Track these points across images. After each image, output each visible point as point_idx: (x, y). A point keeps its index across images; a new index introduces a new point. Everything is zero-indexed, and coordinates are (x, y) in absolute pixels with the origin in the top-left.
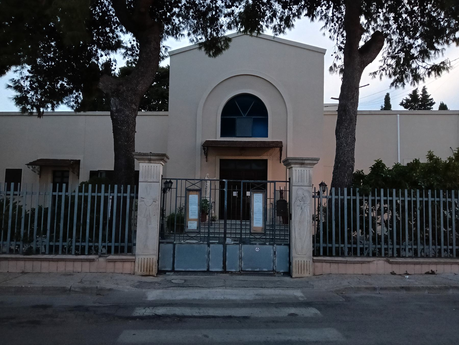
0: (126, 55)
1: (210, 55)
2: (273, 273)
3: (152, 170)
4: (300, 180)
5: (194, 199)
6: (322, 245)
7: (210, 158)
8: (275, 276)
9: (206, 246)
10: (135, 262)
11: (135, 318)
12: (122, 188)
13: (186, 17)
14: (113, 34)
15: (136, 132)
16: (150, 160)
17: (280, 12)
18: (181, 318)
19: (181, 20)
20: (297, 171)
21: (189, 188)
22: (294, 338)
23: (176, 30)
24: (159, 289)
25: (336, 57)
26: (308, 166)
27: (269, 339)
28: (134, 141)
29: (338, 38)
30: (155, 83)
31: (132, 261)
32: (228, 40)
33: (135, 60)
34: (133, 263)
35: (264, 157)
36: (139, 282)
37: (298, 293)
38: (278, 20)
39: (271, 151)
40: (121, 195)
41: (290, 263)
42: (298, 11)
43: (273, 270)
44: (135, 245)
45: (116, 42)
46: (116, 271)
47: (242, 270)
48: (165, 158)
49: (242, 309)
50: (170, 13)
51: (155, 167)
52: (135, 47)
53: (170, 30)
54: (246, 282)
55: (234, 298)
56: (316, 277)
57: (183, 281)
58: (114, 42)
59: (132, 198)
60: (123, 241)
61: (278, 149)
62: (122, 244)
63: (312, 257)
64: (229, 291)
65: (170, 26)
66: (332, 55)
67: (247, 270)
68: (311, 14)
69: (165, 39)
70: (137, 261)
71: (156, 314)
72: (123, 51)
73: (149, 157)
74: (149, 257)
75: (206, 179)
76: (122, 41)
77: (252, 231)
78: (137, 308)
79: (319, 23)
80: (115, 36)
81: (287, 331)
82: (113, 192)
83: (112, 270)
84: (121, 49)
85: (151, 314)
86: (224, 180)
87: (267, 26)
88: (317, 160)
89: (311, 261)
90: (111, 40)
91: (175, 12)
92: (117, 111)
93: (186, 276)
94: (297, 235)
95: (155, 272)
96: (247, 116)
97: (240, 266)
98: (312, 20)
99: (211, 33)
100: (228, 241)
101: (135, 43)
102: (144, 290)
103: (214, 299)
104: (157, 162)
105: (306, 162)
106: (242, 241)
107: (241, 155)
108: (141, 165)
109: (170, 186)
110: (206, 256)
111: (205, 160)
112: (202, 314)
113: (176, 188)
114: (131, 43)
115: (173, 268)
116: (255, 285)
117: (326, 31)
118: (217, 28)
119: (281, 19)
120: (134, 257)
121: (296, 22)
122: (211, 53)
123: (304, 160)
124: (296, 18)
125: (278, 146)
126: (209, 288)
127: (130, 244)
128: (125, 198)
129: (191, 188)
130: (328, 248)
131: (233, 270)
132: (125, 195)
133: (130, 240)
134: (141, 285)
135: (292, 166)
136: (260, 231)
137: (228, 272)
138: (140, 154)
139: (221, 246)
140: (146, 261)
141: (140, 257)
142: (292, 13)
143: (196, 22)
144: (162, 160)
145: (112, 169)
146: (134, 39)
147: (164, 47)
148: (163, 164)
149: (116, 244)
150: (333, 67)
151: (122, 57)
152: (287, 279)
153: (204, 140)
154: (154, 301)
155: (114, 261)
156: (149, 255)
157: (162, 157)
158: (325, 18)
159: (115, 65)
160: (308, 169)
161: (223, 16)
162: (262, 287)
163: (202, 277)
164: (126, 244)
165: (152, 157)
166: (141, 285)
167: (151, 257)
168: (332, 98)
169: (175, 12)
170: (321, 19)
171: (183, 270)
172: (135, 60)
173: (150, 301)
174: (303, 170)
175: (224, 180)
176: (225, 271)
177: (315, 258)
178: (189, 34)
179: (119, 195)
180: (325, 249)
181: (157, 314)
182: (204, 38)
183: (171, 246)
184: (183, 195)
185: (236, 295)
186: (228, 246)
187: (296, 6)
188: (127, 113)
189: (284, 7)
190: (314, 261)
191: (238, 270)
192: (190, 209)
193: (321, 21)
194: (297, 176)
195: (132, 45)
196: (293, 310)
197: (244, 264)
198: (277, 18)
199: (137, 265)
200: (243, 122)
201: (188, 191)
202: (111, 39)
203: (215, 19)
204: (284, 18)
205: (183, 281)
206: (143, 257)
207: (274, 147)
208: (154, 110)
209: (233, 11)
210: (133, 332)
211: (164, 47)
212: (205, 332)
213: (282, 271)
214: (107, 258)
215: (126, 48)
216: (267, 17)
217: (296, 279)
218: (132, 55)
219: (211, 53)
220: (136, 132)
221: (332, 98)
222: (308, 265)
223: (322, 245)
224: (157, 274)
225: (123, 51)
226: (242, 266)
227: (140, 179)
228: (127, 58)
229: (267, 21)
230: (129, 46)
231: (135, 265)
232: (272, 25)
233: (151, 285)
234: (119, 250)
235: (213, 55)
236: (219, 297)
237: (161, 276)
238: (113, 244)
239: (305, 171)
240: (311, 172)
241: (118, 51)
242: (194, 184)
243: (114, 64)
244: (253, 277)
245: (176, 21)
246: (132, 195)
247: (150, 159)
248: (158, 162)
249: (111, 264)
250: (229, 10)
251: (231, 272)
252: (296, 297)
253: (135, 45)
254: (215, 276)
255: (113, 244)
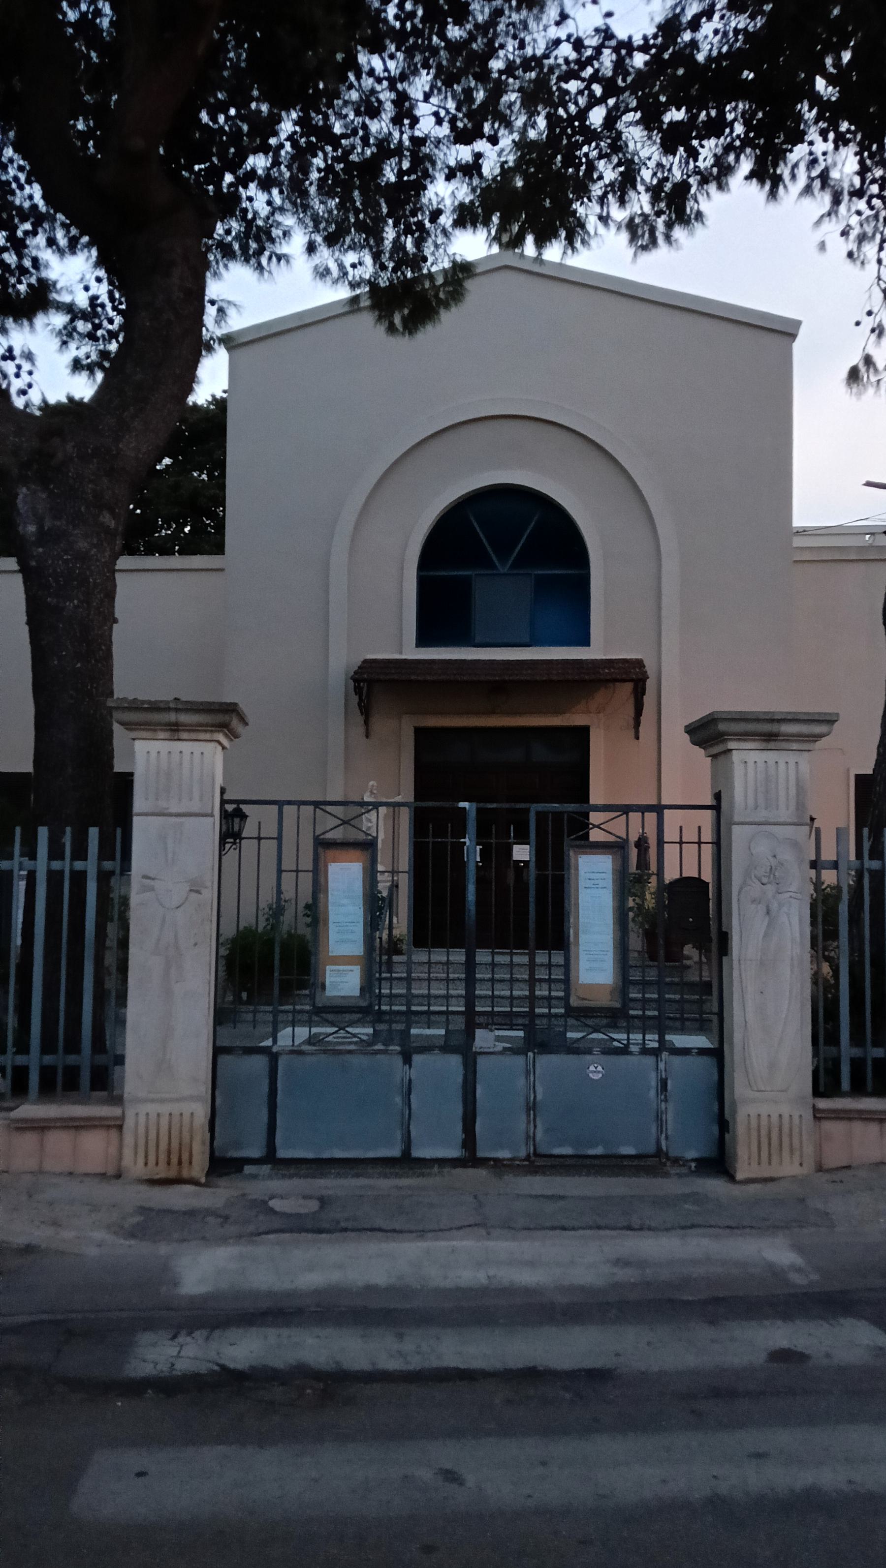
0: (70, 335)
1: (391, 329)
2: (653, 1162)
3: (186, 765)
4: (761, 801)
5: (345, 878)
6: (847, 1050)
7: (379, 724)
8: (666, 1175)
9: (398, 1061)
10: (120, 1128)
11: (136, 1388)
12: (67, 840)
13: (296, 191)
14: (20, 256)
15: (115, 621)
16: (175, 730)
17: (652, 164)
18: (332, 1386)
19: (278, 200)
20: (751, 764)
21: (329, 836)
22: (830, 1478)
23: (258, 240)
24: (224, 1240)
25: (873, 331)
26: (795, 746)
27: (723, 1489)
28: (109, 655)
29: (882, 254)
30: (167, 461)
31: (109, 1127)
32: (462, 271)
33: (104, 354)
34: (114, 1133)
35: (578, 720)
36: (143, 1210)
37: (777, 1253)
38: (645, 198)
39: (600, 697)
40: (65, 865)
41: (724, 1125)
42: (719, 161)
43: (659, 1152)
44: (120, 1060)
45: (30, 286)
46: (48, 1165)
47: (536, 1154)
48: (235, 722)
49: (253, 1056)
50: (233, 172)
51: (197, 755)
52: (103, 306)
53: (236, 238)
54: (561, 1203)
55: (526, 1278)
56: (827, 1177)
57: (314, 1205)
58: (22, 288)
59: (104, 878)
60: (73, 1046)
61: (629, 686)
62: (72, 1059)
63: (810, 1099)
64: (502, 1246)
65: (235, 225)
66: (858, 324)
67: (557, 1151)
68: (766, 174)
69: (215, 274)
70: (129, 1123)
71: (223, 1367)
72: (59, 320)
73: (172, 717)
74: (175, 1108)
75: (366, 799)
76: (55, 283)
77: (574, 1002)
78: (145, 1338)
79: (799, 208)
80: (27, 263)
81: (783, 1438)
82: (33, 856)
83: (32, 1164)
84: (52, 311)
85: (203, 1368)
86: (462, 804)
87: (604, 219)
88: (830, 720)
89: (808, 1115)
90: (13, 280)
91: (253, 170)
92: (44, 537)
93: (322, 1182)
94: (750, 1016)
95: (199, 1167)
96: (513, 567)
97: (530, 1138)
98: (773, 194)
99: (396, 241)
100: (483, 1039)
101: (102, 290)
102: (164, 1249)
103: (448, 1284)
104: (202, 736)
105: (786, 728)
106: (539, 1041)
107: (492, 712)
108: (141, 747)
109: (236, 828)
110: (398, 1100)
111: (361, 730)
112: (415, 1363)
113: (279, 839)
114: (87, 289)
115: (271, 1146)
116: (600, 1220)
117: (833, 228)
118: (420, 224)
119: (655, 192)
120: (116, 1111)
121: (710, 202)
122: (397, 320)
123: (779, 721)
124: (712, 188)
125: (632, 677)
126: (422, 1234)
127: (101, 1059)
128: (79, 878)
129: (336, 835)
130: (869, 1063)
131: (504, 1154)
132: (79, 865)
133: (99, 1043)
134: (149, 1224)
135: (731, 745)
136: (604, 1000)
137: (482, 1162)
138: (135, 706)
139: (455, 1061)
140: (164, 1122)
141: (144, 1109)
142: (697, 171)
143: (333, 203)
144: (223, 727)
145: (27, 767)
146: (102, 273)
147: (213, 303)
148: (225, 742)
149: (48, 1059)
150: (862, 369)
151: (56, 342)
152: (715, 1186)
153: (357, 661)
154: (206, 1298)
155: (40, 1127)
156: (178, 1100)
157: (222, 717)
158: (823, 188)
159: (30, 373)
160: (792, 758)
161: (440, 177)
162: (629, 1228)
163: (384, 1184)
164: (85, 1058)
165: (184, 718)
166: (149, 1224)
167: (187, 1108)
168: (869, 484)
169: (253, 170)
170: (808, 190)
171: (310, 1155)
172: (104, 354)
173: (192, 1299)
174: (771, 763)
175: (462, 804)
176: (470, 1158)
177: (823, 1104)
178: (311, 248)
179: (56, 865)
180: (857, 1065)
181: (232, 1366)
182: (368, 260)
183: (259, 1063)
184: (307, 863)
185: (531, 1264)
186: (482, 1063)
187: (713, 142)
188: (83, 545)
189: (668, 148)
190: (818, 1115)
191: (522, 1154)
192: (332, 917)
193: (807, 201)
194: (751, 783)
195: (93, 299)
196: (780, 1335)
197: (547, 1131)
198: (641, 188)
199: (129, 1139)
200: (498, 591)
201: (324, 845)
202: (12, 274)
203: (409, 190)
204: (668, 186)
205: (314, 1205)
206: (152, 1108)
207: (615, 680)
208: (166, 551)
209: (478, 156)
210: (135, 1459)
211: (213, 303)
212: (447, 1454)
213: (692, 1154)
214: (14, 1114)
215: (70, 309)
216: (601, 184)
217: (752, 1188)
218: (92, 336)
219: (397, 320)
220: (115, 621)
221: (869, 484)
222: (796, 1131)
223: (847, 1050)
224: (208, 1174)
225: (59, 320)
226: (538, 1139)
227: (139, 803)
228: (73, 345)
229: (602, 200)
230: (82, 300)
231: (121, 1140)
232: (619, 214)
233: (189, 1225)
234: (58, 1083)
235: (405, 327)
236: (469, 1276)
237: (223, 1182)
238: (34, 1060)
239: (782, 766)
240: (805, 767)
241: (40, 320)
242: (344, 822)
243: (26, 366)
244: (591, 1179)
245: (257, 200)
246: (108, 865)
247: (176, 724)
248: (208, 736)
249: (29, 1140)
250: (464, 153)
251: (496, 1160)
252: (776, 1272)
253: (104, 298)
254: (434, 1180)
255: (34, 1060)
